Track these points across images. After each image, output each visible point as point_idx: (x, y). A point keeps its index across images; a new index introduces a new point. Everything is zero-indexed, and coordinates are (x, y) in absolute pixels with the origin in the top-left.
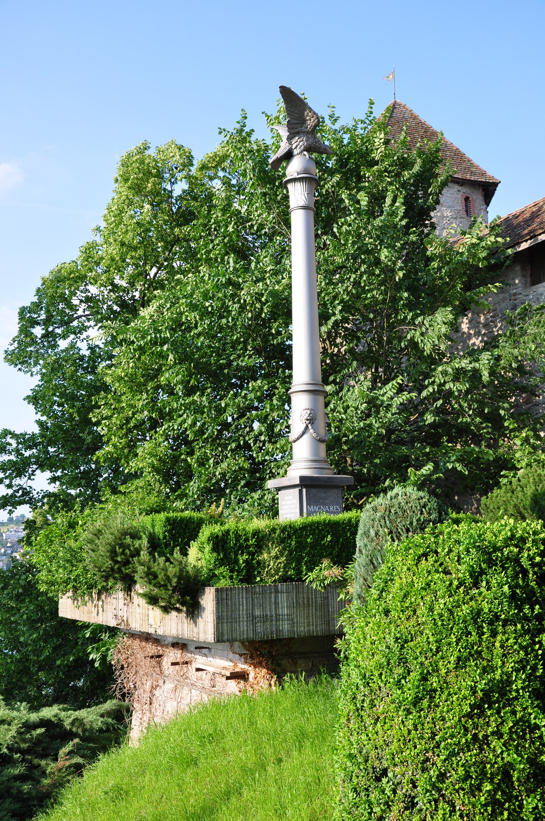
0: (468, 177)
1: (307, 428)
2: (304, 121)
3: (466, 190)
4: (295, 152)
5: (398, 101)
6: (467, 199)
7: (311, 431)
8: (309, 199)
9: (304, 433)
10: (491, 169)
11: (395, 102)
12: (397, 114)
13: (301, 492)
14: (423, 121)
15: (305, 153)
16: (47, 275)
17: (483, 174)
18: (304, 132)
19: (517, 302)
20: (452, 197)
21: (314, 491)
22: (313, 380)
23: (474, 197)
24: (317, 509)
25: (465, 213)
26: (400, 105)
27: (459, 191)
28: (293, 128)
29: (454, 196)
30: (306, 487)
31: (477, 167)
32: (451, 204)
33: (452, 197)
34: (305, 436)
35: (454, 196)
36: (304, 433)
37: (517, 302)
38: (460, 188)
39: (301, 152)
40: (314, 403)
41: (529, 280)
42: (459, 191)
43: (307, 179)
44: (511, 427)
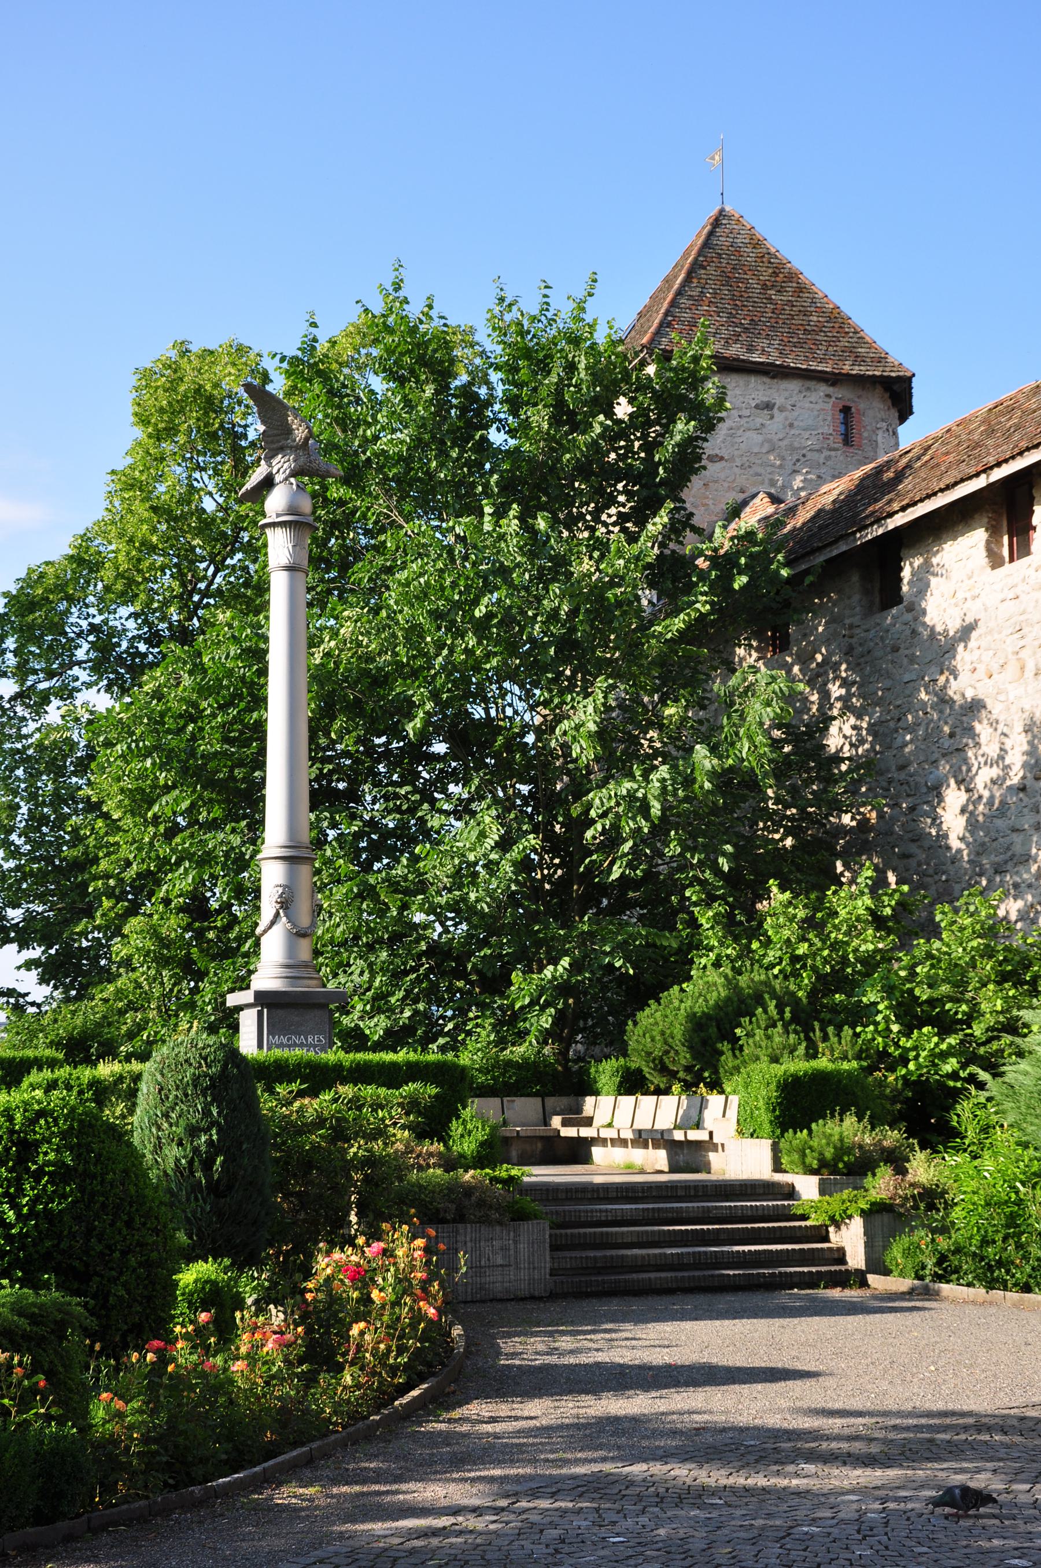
0: (846, 368)
1: (277, 915)
2: (288, 431)
3: (843, 394)
4: (278, 478)
5: (727, 208)
6: (846, 410)
7: (284, 919)
8: (294, 554)
9: (273, 923)
10: (898, 345)
11: (722, 211)
12: (722, 240)
13: (260, 1014)
14: (773, 250)
15: (292, 480)
16: (464, 306)
17: (881, 359)
18: (291, 447)
19: (853, 641)
20: (812, 410)
21: (280, 1013)
22: (291, 840)
23: (862, 406)
24: (285, 1041)
25: (840, 438)
26: (730, 217)
27: (828, 396)
28: (272, 442)
29: (818, 407)
30: (269, 1006)
31: (870, 345)
32: (810, 422)
33: (812, 410)
34: (275, 927)
35: (818, 407)
36: (273, 923)
37: (853, 641)
38: (830, 390)
39: (286, 479)
40: (292, 876)
41: (877, 600)
42: (828, 396)
43: (296, 524)
44: (694, 898)
